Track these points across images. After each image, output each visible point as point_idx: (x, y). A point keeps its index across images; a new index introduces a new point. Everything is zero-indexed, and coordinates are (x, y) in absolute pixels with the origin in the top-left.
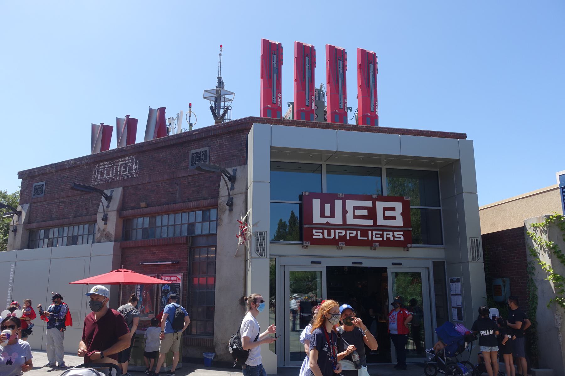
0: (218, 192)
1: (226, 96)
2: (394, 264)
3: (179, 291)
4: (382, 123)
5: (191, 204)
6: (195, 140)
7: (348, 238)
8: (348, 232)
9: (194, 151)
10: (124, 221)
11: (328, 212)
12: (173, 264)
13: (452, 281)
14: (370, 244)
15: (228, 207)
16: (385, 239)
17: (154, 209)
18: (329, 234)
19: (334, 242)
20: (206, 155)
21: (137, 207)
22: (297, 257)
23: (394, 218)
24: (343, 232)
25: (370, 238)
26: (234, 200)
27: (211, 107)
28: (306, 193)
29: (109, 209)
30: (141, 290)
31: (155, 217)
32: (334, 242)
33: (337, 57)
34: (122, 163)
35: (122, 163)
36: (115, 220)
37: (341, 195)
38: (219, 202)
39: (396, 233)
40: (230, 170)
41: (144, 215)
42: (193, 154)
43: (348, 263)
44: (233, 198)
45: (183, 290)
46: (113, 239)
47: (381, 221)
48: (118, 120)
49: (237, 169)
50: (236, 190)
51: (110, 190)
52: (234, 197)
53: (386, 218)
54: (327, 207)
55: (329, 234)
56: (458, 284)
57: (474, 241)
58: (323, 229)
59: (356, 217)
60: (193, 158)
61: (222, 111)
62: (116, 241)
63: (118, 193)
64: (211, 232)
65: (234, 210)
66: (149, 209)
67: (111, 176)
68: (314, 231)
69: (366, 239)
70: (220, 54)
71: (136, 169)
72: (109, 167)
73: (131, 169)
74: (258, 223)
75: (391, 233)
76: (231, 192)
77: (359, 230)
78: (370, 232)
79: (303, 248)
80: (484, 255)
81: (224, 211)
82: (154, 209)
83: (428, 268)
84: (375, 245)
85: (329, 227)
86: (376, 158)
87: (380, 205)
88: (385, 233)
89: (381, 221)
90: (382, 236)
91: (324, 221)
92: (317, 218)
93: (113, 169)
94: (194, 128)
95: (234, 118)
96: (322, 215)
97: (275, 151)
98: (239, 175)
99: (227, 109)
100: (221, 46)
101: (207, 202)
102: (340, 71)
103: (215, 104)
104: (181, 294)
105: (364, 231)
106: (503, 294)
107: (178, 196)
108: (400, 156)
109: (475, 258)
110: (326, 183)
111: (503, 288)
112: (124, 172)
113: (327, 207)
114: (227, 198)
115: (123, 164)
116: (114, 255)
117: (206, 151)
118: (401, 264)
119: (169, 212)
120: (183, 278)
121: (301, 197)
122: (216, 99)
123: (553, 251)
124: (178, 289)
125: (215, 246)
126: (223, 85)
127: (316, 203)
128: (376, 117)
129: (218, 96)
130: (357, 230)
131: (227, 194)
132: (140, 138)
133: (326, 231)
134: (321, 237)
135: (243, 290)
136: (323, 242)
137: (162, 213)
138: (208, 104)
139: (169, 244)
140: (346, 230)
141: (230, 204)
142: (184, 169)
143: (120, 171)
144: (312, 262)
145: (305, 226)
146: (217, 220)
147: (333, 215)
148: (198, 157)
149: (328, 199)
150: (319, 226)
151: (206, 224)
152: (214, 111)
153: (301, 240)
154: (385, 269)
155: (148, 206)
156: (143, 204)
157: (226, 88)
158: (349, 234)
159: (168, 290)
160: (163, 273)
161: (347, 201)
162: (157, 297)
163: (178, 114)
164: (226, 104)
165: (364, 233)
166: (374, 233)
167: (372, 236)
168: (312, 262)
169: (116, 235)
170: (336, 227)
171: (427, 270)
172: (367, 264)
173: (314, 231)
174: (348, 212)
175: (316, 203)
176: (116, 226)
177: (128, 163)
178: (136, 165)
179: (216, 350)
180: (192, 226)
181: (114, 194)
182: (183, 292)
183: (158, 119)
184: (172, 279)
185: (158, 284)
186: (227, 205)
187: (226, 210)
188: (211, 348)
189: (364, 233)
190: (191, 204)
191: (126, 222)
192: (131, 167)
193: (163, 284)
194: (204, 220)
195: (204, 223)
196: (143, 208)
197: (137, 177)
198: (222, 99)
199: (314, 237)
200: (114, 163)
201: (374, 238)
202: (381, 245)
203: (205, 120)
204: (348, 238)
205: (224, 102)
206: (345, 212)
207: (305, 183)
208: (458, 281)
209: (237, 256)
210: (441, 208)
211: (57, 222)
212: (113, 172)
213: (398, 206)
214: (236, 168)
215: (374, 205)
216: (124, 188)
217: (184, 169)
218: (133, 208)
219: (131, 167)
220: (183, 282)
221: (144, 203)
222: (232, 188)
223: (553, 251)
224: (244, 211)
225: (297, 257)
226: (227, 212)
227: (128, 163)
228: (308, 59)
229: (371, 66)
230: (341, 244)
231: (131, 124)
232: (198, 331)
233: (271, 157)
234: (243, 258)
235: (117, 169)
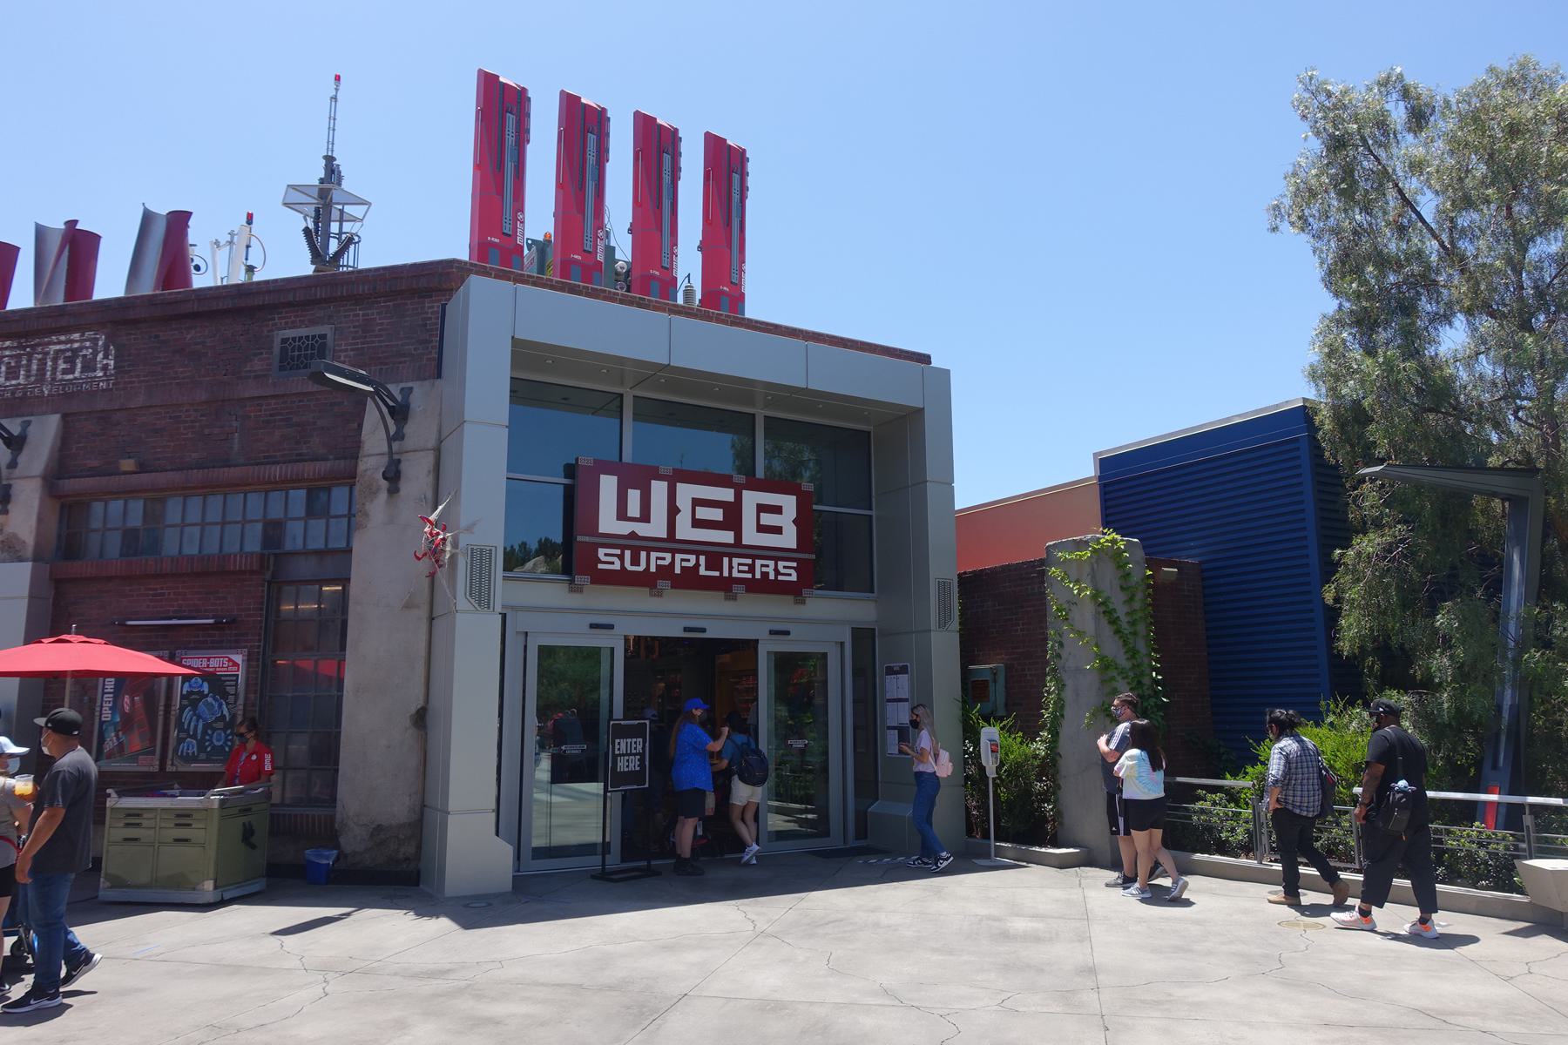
0: (358, 445)
1: (347, 209)
2: (772, 632)
3: (236, 695)
4: (752, 311)
5: (277, 471)
6: (289, 304)
7: (678, 570)
8: (678, 557)
9: (290, 333)
10: (63, 506)
11: (634, 509)
12: (217, 625)
13: (890, 671)
14: (725, 586)
15: (384, 484)
16: (758, 576)
17: (161, 478)
18: (635, 562)
19: (645, 580)
20: (323, 347)
21: (112, 471)
22: (560, 613)
23: (777, 530)
24: (668, 556)
25: (726, 574)
26: (404, 467)
27: (307, 231)
28: (586, 461)
29: (17, 472)
30: (117, 693)
31: (163, 501)
32: (645, 580)
33: (656, 143)
34: (62, 347)
35: (62, 347)
36: (36, 503)
37: (665, 469)
38: (362, 466)
39: (781, 564)
40: (395, 389)
41: (128, 493)
42: (284, 341)
43: (674, 630)
44: (399, 461)
45: (247, 691)
46: (29, 551)
47: (750, 536)
48: (41, 233)
49: (411, 389)
50: (409, 443)
51: (19, 420)
52: (403, 458)
53: (762, 529)
54: (634, 496)
55: (635, 562)
56: (904, 678)
57: (943, 586)
58: (623, 548)
59: (697, 523)
60: (283, 350)
61: (333, 246)
62: (37, 558)
63: (45, 431)
64: (331, 546)
65: (402, 492)
66: (145, 478)
67: (22, 380)
68: (601, 552)
69: (717, 574)
70: (335, 98)
71: (105, 368)
72: (19, 357)
73: (89, 366)
74: (474, 524)
75: (771, 563)
76: (396, 446)
77: (703, 553)
78: (726, 560)
79: (571, 590)
80: (961, 616)
81: (374, 493)
82: (161, 478)
83: (842, 644)
84: (736, 588)
85: (636, 545)
86: (743, 388)
87: (751, 499)
88: (759, 562)
89: (750, 536)
90: (752, 569)
91: (624, 528)
92: (608, 522)
93: (30, 361)
94: (257, 277)
95: (363, 265)
96: (622, 515)
97: (523, 352)
98: (417, 401)
99: (348, 242)
100: (338, 78)
101: (322, 467)
102: (667, 178)
103: (316, 224)
104: (241, 701)
105: (714, 556)
106: (992, 698)
107: (236, 447)
108: (806, 391)
109: (943, 624)
110: (633, 440)
111: (991, 688)
112: (65, 372)
113: (634, 496)
114: (385, 459)
115: (63, 351)
116: (31, 597)
117: (323, 337)
118: (787, 633)
119: (207, 489)
120: (249, 659)
121: (570, 470)
122: (317, 210)
123: (1102, 609)
124: (231, 690)
125: (345, 581)
126: (340, 178)
127: (608, 485)
128: (741, 297)
129: (324, 203)
130: (698, 554)
131: (385, 449)
132: (110, 282)
133: (628, 553)
134: (617, 566)
135: (423, 689)
136: (621, 578)
137: (186, 491)
138: (298, 222)
139: (210, 572)
140: (673, 552)
141: (393, 475)
142: (256, 377)
143: (54, 369)
144: (592, 626)
145: (579, 538)
146: (350, 515)
147: (645, 517)
148: (300, 349)
149: (636, 477)
150: (612, 541)
151: (318, 525)
152: (314, 238)
153: (567, 570)
154: (752, 645)
155: (142, 468)
156: (127, 464)
157: (345, 185)
158: (682, 562)
159: (201, 693)
160: (187, 647)
161: (679, 486)
162: (168, 706)
163: (232, 234)
164: (347, 227)
165: (714, 562)
166: (736, 561)
167: (731, 568)
168: (592, 626)
169: (37, 544)
170: (652, 544)
171: (522, 637)
172: (715, 631)
173: (601, 552)
174: (676, 512)
175: (608, 485)
176: (40, 520)
177: (81, 349)
178: (106, 357)
179: (342, 840)
180: (273, 531)
181: (31, 430)
182: (246, 699)
183: (168, 237)
184: (214, 663)
185: (171, 676)
186: (385, 478)
187: (378, 490)
188: (329, 834)
189: (714, 562)
190: (277, 471)
191: (67, 509)
192: (92, 361)
193: (187, 678)
194: (311, 513)
195: (312, 522)
196: (125, 473)
197: (108, 390)
198: (335, 214)
199: (600, 566)
200: (33, 347)
201: (735, 574)
202: (748, 591)
203: (285, 258)
204: (678, 570)
205: (341, 221)
206: (673, 511)
207: (585, 435)
208: (904, 670)
209: (408, 606)
210: (873, 513)
211: (197, 475)
212: (28, 371)
213: (789, 503)
214: (410, 384)
215: (738, 497)
216: (65, 416)
217: (256, 377)
218: (94, 473)
219: (92, 361)
220: (248, 672)
221: (132, 461)
222: (399, 436)
223: (1102, 609)
224: (430, 495)
225: (560, 613)
226: (383, 495)
227: (81, 349)
228: (592, 138)
229: (736, 177)
230: (661, 584)
231: (79, 247)
232: (288, 794)
233: (514, 366)
234: (423, 612)
235: (42, 363)
